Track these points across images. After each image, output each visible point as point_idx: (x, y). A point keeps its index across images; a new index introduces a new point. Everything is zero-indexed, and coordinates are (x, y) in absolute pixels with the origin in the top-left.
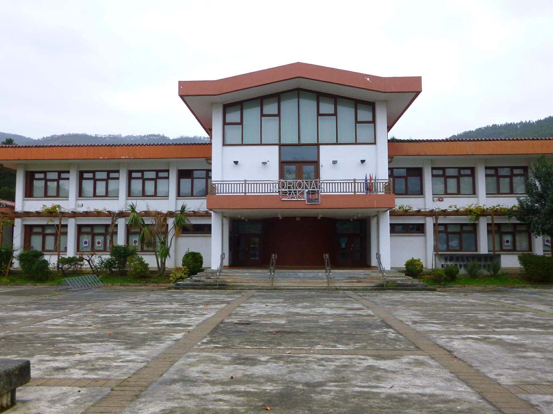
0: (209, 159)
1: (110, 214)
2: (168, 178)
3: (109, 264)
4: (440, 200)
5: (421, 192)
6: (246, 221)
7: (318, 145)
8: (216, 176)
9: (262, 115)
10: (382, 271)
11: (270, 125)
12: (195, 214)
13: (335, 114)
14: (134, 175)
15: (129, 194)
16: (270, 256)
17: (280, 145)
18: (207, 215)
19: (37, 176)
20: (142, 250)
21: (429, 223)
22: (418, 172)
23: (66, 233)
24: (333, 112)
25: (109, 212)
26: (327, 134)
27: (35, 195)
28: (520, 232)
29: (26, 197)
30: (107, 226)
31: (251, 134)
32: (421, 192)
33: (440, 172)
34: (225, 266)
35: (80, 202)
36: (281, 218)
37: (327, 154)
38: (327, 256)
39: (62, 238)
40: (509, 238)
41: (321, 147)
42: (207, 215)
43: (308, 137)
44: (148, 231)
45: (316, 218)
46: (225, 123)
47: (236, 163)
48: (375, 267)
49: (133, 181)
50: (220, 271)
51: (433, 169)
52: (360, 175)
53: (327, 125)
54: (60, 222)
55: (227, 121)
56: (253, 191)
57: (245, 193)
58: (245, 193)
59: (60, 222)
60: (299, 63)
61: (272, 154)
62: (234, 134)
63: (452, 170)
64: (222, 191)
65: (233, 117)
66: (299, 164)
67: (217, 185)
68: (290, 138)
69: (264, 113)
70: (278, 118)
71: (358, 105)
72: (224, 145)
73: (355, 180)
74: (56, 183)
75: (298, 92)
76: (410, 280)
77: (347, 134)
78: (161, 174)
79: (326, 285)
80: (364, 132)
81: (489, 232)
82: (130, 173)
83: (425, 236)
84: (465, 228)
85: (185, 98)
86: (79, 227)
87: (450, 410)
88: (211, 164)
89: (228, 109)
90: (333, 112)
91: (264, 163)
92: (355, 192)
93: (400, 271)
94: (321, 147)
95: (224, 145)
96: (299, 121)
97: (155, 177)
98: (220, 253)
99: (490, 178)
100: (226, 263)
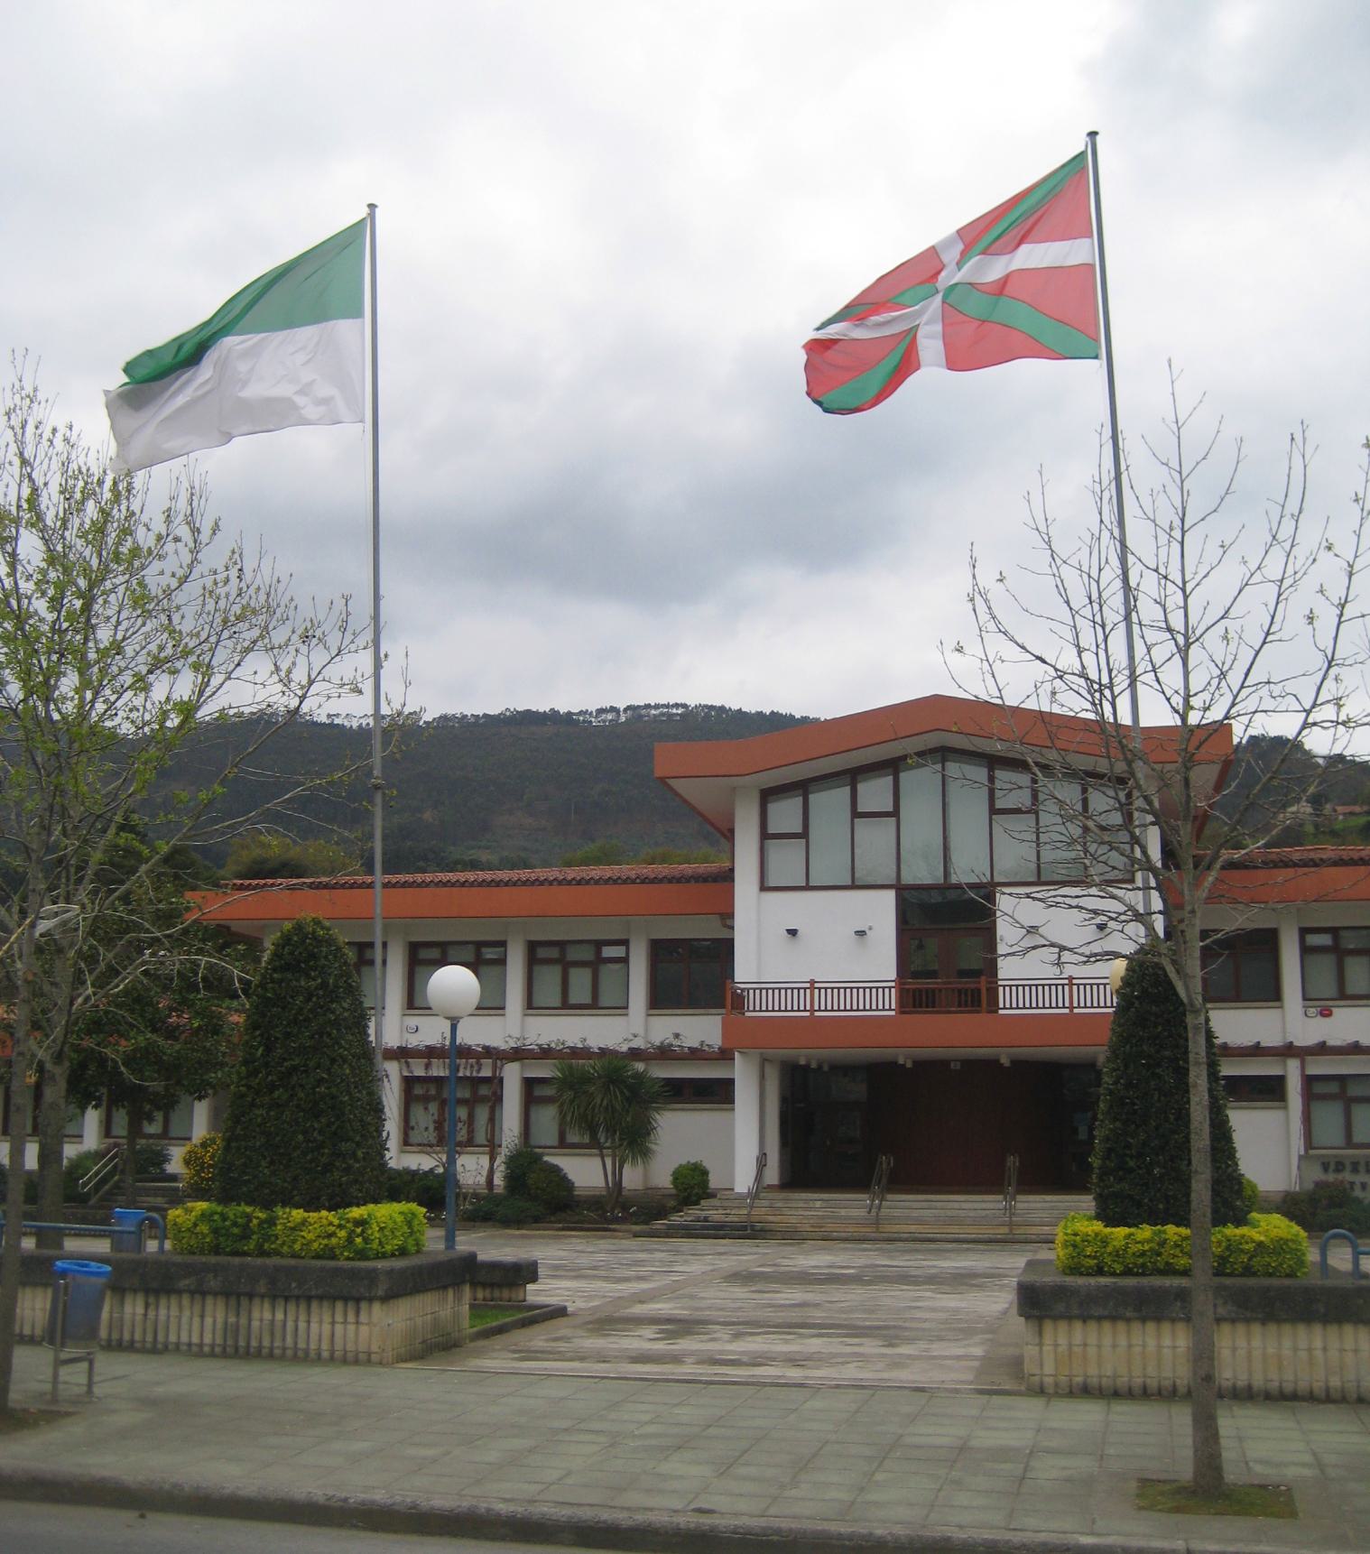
0: (727, 916)
1: (488, 1052)
2: (625, 960)
4: (1325, 1013)
5: (1271, 993)
6: (826, 1068)
8: (745, 970)
11: (875, 841)
12: (696, 1055)
14: (542, 953)
18: (725, 1055)
20: (563, 1144)
21: (1293, 1073)
22: (1266, 942)
25: (485, 1047)
28: (1324, 1097)
31: (830, 862)
32: (1271, 993)
33: (1325, 940)
34: (769, 1186)
35: (413, 1021)
36: (909, 1065)
38: (1012, 1161)
40: (462, 1113)
42: (725, 1055)
43: (968, 867)
44: (614, 1100)
45: (992, 1064)
46: (765, 835)
47: (793, 932)
50: (755, 1195)
51: (1304, 932)
55: (771, 830)
56: (829, 1007)
57: (812, 1010)
58: (812, 1010)
60: (937, 698)
61: (881, 911)
62: (786, 861)
64: (757, 1008)
65: (785, 814)
66: (945, 931)
68: (922, 871)
72: (764, 888)
78: (608, 952)
79: (1005, 1230)
82: (532, 947)
83: (1286, 1108)
88: (732, 928)
91: (861, 933)
92: (1071, 1008)
95: (764, 888)
100: (772, 1176)
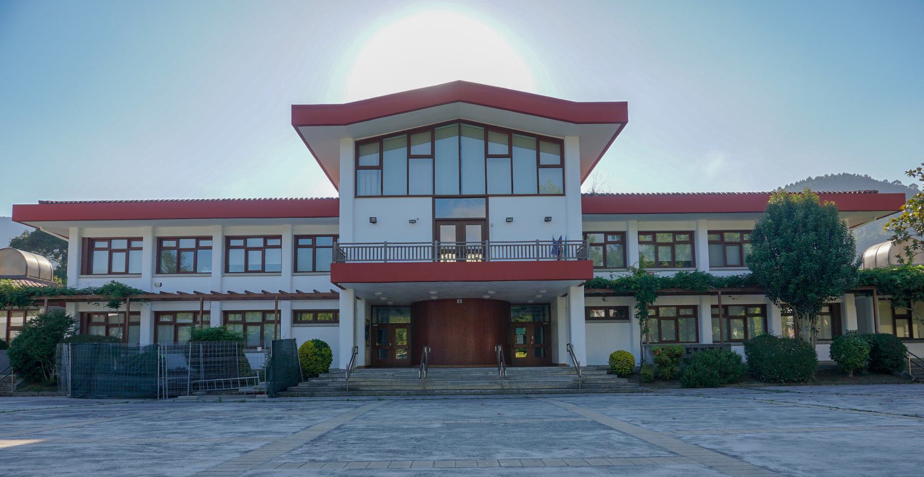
3: (63, 330)
7: (486, 197)
9: (410, 156)
10: (577, 369)
11: (421, 169)
13: (510, 156)
15: (226, 269)
16: (422, 349)
17: (435, 197)
19: (98, 245)
23: (138, 324)
24: (507, 153)
26: (499, 183)
27: (95, 270)
29: (82, 273)
30: (195, 313)
31: (395, 183)
34: (359, 367)
37: (499, 208)
39: (132, 329)
41: (490, 198)
42: (334, 296)
43: (473, 186)
46: (358, 167)
48: (564, 365)
49: (231, 251)
50: (349, 371)
52: (547, 234)
53: (499, 169)
54: (128, 308)
59: (128, 308)
61: (423, 209)
62: (369, 181)
63: (666, 235)
67: (345, 250)
68: (447, 186)
69: (412, 154)
70: (431, 160)
71: (543, 144)
73: (537, 241)
74: (259, 327)
75: (460, 125)
76: (613, 380)
77: (525, 182)
78: (270, 242)
80: (550, 179)
81: (714, 316)
84: (682, 312)
85: (300, 128)
86: (157, 315)
87: (518, 474)
89: (362, 148)
90: (507, 153)
93: (599, 368)
94: (490, 198)
95: (356, 196)
96: (460, 163)
97: (262, 245)
98: (351, 345)
99: (714, 246)
